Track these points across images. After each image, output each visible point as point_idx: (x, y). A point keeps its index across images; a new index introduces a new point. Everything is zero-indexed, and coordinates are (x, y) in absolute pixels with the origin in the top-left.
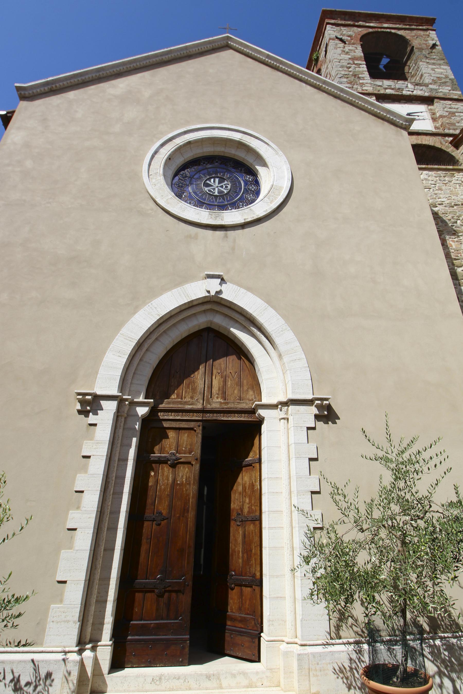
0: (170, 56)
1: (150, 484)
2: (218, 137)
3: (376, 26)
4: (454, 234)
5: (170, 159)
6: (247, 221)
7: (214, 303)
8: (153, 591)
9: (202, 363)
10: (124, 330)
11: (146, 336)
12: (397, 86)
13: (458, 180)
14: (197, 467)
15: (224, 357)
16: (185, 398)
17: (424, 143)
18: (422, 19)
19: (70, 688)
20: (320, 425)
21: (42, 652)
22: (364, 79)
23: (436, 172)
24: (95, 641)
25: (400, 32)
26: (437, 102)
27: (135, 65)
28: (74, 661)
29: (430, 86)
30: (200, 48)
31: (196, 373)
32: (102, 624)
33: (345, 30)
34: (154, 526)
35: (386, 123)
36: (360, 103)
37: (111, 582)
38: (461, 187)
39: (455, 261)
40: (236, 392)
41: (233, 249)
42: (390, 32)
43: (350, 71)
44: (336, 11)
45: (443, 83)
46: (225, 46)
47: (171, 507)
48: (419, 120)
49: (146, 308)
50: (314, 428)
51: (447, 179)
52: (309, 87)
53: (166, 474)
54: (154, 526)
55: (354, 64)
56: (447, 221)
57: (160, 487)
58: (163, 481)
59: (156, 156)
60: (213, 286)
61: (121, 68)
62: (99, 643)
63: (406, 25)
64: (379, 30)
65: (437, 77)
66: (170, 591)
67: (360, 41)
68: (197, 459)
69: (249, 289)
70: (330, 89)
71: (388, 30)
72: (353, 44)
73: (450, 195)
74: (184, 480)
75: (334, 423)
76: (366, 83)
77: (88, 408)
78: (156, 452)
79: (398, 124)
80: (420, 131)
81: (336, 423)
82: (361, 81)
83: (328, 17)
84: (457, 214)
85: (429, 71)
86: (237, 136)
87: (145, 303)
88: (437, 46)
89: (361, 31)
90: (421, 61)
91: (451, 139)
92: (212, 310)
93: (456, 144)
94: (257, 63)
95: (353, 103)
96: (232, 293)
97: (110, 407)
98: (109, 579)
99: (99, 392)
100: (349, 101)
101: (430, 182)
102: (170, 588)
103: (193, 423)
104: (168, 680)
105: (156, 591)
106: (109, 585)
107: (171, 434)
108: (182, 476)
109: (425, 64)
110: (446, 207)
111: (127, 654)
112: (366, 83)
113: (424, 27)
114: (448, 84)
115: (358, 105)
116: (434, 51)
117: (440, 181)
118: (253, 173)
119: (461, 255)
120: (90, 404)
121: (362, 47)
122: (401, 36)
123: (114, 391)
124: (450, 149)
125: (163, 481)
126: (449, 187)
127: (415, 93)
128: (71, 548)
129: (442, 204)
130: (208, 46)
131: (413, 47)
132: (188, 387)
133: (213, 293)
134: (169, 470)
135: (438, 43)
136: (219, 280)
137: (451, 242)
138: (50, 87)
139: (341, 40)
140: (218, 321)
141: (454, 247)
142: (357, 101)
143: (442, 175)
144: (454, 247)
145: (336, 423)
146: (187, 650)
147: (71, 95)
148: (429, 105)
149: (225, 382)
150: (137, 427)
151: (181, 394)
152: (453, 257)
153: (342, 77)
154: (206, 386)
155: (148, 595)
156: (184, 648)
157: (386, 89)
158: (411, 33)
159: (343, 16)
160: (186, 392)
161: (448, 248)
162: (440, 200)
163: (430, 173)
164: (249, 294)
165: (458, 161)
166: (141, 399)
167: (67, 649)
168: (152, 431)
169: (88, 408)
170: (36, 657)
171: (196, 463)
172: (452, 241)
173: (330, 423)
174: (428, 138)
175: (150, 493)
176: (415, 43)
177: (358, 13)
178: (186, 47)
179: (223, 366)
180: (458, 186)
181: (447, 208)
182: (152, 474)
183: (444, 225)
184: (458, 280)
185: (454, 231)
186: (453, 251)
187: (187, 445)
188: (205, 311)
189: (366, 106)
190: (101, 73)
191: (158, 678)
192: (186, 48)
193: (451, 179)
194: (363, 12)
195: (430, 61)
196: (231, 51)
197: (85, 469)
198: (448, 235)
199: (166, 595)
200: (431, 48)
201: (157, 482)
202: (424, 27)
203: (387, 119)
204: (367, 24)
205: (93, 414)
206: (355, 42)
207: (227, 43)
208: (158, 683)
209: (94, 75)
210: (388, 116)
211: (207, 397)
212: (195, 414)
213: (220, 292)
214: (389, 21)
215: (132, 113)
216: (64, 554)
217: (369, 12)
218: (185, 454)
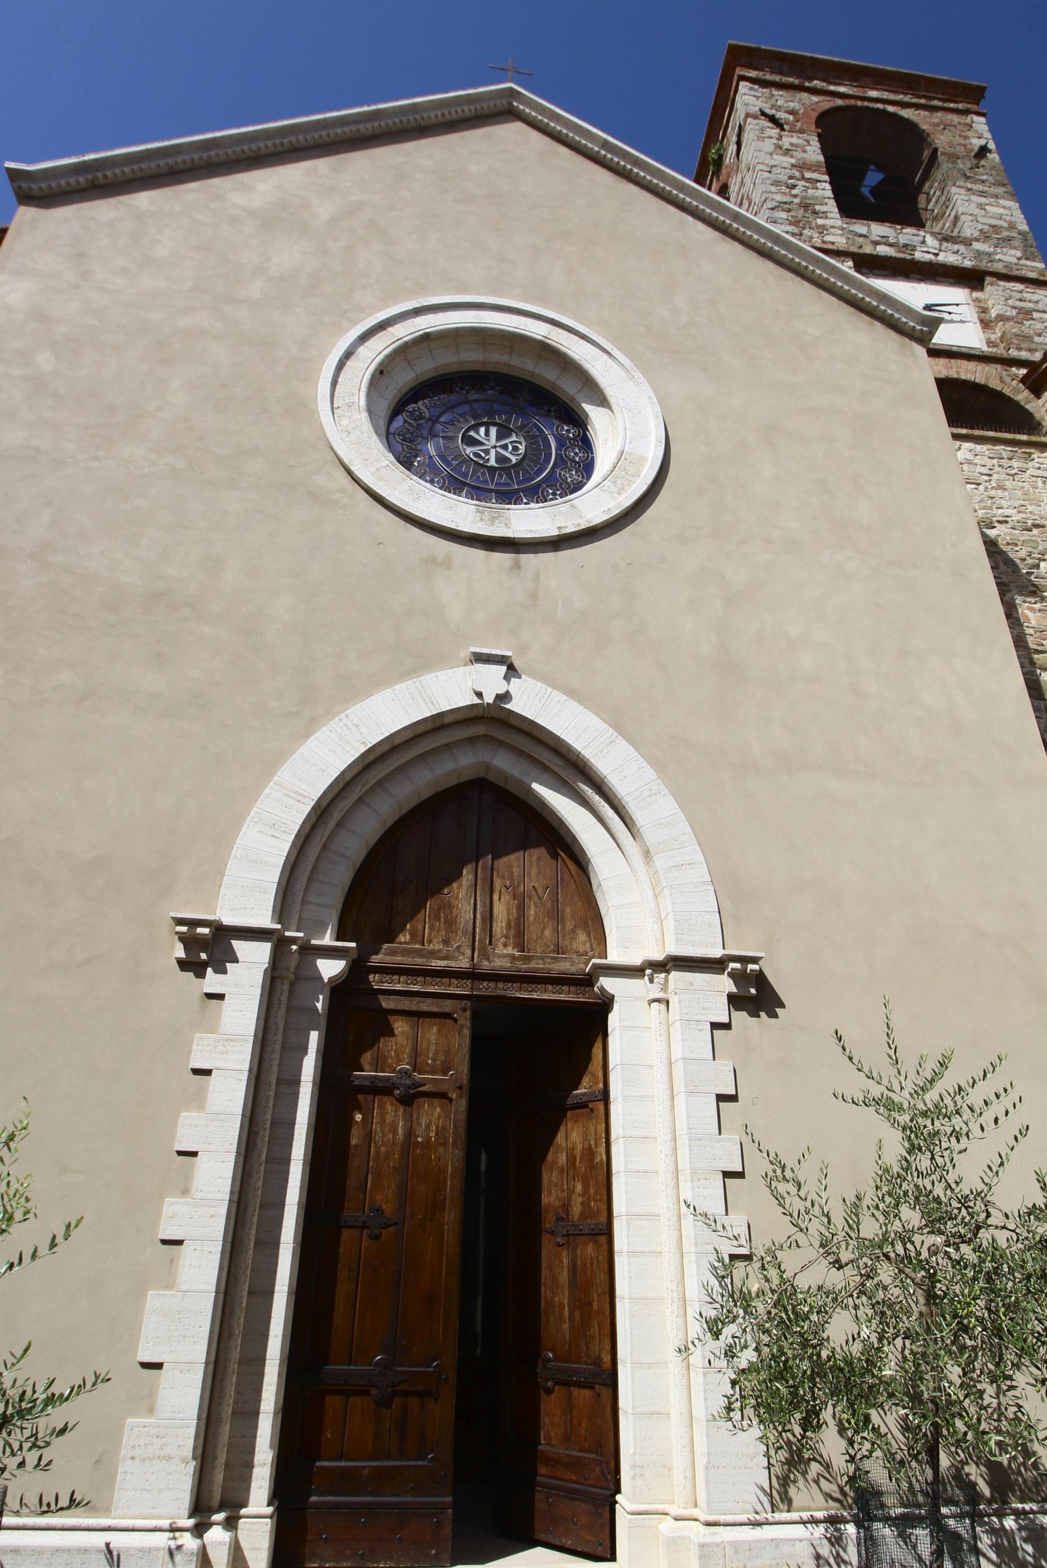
1: (354, 1141)
4: (1033, 594)
5: (381, 372)
7: (491, 723)
8: (367, 1393)
12: (902, 239)
13: (1039, 468)
18: (954, 85)
20: (740, 1018)
22: (826, 218)
23: (991, 447)
24: (233, 1506)
26: (992, 284)
31: (455, 885)
32: (249, 1465)
37: (267, 1370)
39: (1035, 656)
41: (534, 596)
42: (884, 111)
44: (759, 49)
46: (502, 111)
48: (952, 321)
52: (700, 226)
53: (389, 1119)
54: (366, 1241)
56: (1018, 561)
57: (377, 1148)
58: (384, 1135)
59: (349, 363)
60: (490, 682)
62: (243, 1511)
63: (920, 97)
65: (990, 226)
69: (572, 693)
70: (749, 233)
71: (880, 106)
73: (1024, 503)
74: (432, 1134)
76: (832, 227)
77: (204, 956)
78: (367, 1067)
80: (954, 349)
86: (537, 330)
87: (330, 714)
89: (817, 103)
90: (954, 185)
91: (1023, 371)
92: (487, 739)
94: (580, 159)
96: (531, 701)
97: (254, 957)
101: (979, 469)
103: (449, 1002)
105: (374, 1392)
106: (262, 1374)
107: (400, 1026)
108: (428, 1126)
112: (832, 227)
113: (960, 106)
115: (815, 277)
120: (208, 947)
121: (820, 141)
123: (265, 919)
124: (1023, 396)
127: (942, 258)
128: (170, 1285)
130: (466, 109)
134: (396, 1111)
137: (1027, 612)
138: (90, 177)
139: (773, 119)
140: (504, 763)
141: (1034, 623)
144: (1034, 623)
146: (447, 1530)
149: (522, 908)
151: (420, 933)
153: (776, 207)
155: (356, 1401)
161: (1021, 625)
162: (1000, 511)
163: (979, 448)
164: (573, 704)
165: (1039, 424)
169: (204, 956)
171: (459, 1097)
172: (1029, 608)
173: (762, 1014)
174: (971, 365)
176: (941, 140)
177: (811, 58)
178: (414, 105)
181: (1017, 532)
182: (358, 1117)
183: (1010, 570)
185: (1034, 585)
187: (436, 1053)
188: (471, 741)
190: (212, 153)
192: (414, 108)
196: (518, 126)
197: (198, 1101)
199: (397, 1402)
200: (976, 156)
201: (369, 1136)
202: (960, 106)
203: (880, 315)
204: (832, 88)
205: (216, 971)
207: (511, 104)
211: (481, 941)
213: (505, 697)
215: (288, 255)
216: (155, 1299)
218: (432, 1073)
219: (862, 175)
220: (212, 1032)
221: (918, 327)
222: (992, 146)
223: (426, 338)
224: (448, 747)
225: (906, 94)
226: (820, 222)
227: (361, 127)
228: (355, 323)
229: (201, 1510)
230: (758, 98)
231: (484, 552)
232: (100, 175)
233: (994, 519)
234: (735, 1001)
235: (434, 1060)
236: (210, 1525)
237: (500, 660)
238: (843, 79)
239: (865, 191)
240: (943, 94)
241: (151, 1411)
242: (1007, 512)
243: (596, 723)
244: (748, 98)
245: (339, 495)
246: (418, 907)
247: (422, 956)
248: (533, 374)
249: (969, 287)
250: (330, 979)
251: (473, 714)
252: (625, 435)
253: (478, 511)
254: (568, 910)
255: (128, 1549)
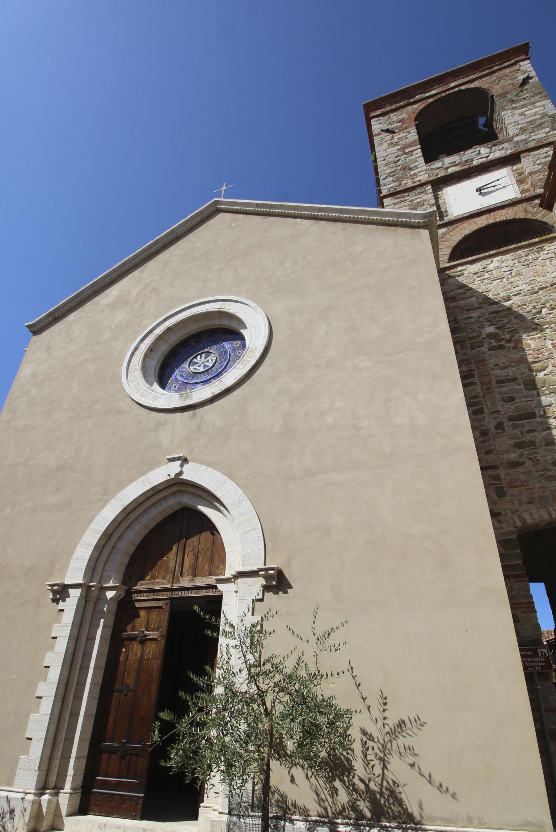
0: (157, 246)
1: (121, 659)
2: (197, 314)
3: (439, 91)
4: (535, 329)
5: (151, 350)
6: (214, 394)
7: (178, 485)
8: (116, 753)
9: (176, 543)
10: (93, 525)
11: (115, 526)
12: (464, 159)
13: (548, 253)
14: (163, 643)
15: (197, 534)
16: (157, 578)
17: (498, 220)
18: (507, 52)
19: (25, 821)
20: (269, 596)
21: (10, 791)
22: (417, 168)
23: (514, 253)
24: (57, 789)
25: (472, 86)
26: (524, 157)
27: (124, 268)
28: (29, 801)
29: (516, 139)
30: (187, 226)
31: (170, 554)
32: (66, 775)
33: (394, 117)
34: (122, 697)
35: (400, 229)
36: (363, 217)
37: (75, 743)
38: (554, 262)
39: (533, 365)
40: (206, 568)
41: (200, 427)
42: (460, 91)
43: (398, 166)
44: (381, 98)
45: (537, 126)
46: (215, 211)
47: (138, 679)
48: (497, 190)
49: (113, 501)
50: (262, 600)
51: (530, 257)
52: (305, 221)
53: (135, 650)
54: (122, 697)
55: (405, 153)
56: (525, 314)
57: (130, 661)
58: (132, 656)
59: (136, 353)
60: (174, 468)
61: (112, 276)
62: (61, 791)
63: (484, 70)
64: (443, 95)
65: (527, 122)
66: (131, 754)
67: (415, 121)
68: (163, 636)
69: (210, 465)
70: (327, 214)
71: (457, 89)
72: (405, 129)
73: (533, 278)
74: (150, 655)
75: (286, 592)
76: (419, 172)
77: (58, 596)
78: (128, 630)
79: (415, 224)
80: (491, 207)
81: (287, 592)
82: (412, 173)
83: (373, 109)
84: (542, 301)
85: (517, 118)
86: (215, 307)
87: (113, 496)
88: (531, 78)
89: (417, 108)
90: (504, 110)
91: (537, 201)
92: (179, 491)
93: (548, 206)
94: (248, 216)
95: (356, 220)
96: (193, 473)
97: (75, 594)
98: (73, 739)
99: (67, 582)
100: (352, 219)
101: (503, 269)
102: (130, 752)
103: (161, 602)
104: (111, 828)
105: (119, 753)
106: (73, 744)
107: (142, 613)
108: (149, 652)
109: (510, 111)
110: (524, 296)
111: (91, 804)
112: (419, 172)
113: (512, 61)
114: (546, 124)
115: (363, 220)
116: (526, 87)
117: (519, 264)
118: (241, 338)
119: (543, 355)
120: (60, 593)
121: (417, 129)
122: (475, 89)
123: (80, 581)
124: (541, 215)
125: (132, 656)
126: (534, 268)
127: (492, 157)
128: (37, 712)
129: (520, 293)
130: (196, 220)
131: (492, 96)
132: (161, 568)
133: (172, 476)
134: (138, 647)
135: (533, 74)
136: (179, 462)
137: (529, 342)
138: (53, 317)
139: (388, 131)
140: (187, 500)
141: (533, 346)
142: (360, 217)
143: (523, 254)
144: (533, 346)
145: (287, 592)
146: (140, 806)
147: (71, 317)
148: (513, 165)
149: (197, 559)
150: (105, 609)
151: (154, 575)
152: (530, 360)
153: (387, 177)
154: (177, 565)
155: (112, 756)
156: (137, 804)
157: (448, 168)
158: (490, 79)
159: (393, 100)
160: (159, 573)
161: (524, 350)
162: (516, 289)
163: (504, 257)
164: (210, 470)
165: (552, 227)
166: (111, 584)
167: (27, 791)
168: (126, 610)
169: (58, 596)
170: (11, 795)
171: (162, 639)
172: (530, 339)
173: (281, 593)
174: (504, 211)
175: (121, 667)
176: (496, 90)
177: (411, 86)
178: (173, 230)
179: (196, 543)
180: (548, 262)
181: (526, 297)
182: (124, 650)
183: (519, 321)
184: (537, 389)
185: (536, 324)
186: (531, 352)
187: (155, 623)
188: (174, 493)
189: (371, 218)
190: (94, 288)
191: (103, 826)
192: (173, 231)
193: (538, 255)
194: (417, 83)
195: (518, 105)
196: (222, 215)
197: (52, 648)
198: (525, 332)
199: (128, 757)
200: (520, 86)
201: (127, 657)
202: (512, 61)
203: (400, 223)
204: (427, 95)
205: (62, 601)
206: (408, 125)
207: (216, 207)
208: (103, 829)
209: (89, 292)
210: (400, 220)
211: (177, 575)
212: (204, 591)
213: (181, 473)
214: (458, 76)
215: (120, 316)
216: (33, 716)
217: (426, 79)
218: (153, 631)
219: (476, 122)
220: (60, 623)
221: (421, 221)
222: (533, 74)
223: (169, 329)
224: (165, 498)
225: (474, 74)
226: (412, 173)
227: (151, 250)
228: (140, 334)
229: (41, 790)
230: (380, 123)
231: (181, 414)
232: (56, 314)
233: (511, 295)
234: (266, 588)
235: (154, 626)
236: (45, 794)
237: (178, 459)
238: (434, 86)
239: (481, 127)
240: (500, 61)
241: (28, 754)
242: (520, 288)
243: (219, 475)
244: (377, 125)
245: (127, 408)
246: (155, 564)
247: (153, 584)
248: (220, 325)
249: (510, 165)
250: (110, 599)
251: (170, 483)
252: (255, 337)
253: (180, 397)
254: (216, 556)
255: (13, 798)
